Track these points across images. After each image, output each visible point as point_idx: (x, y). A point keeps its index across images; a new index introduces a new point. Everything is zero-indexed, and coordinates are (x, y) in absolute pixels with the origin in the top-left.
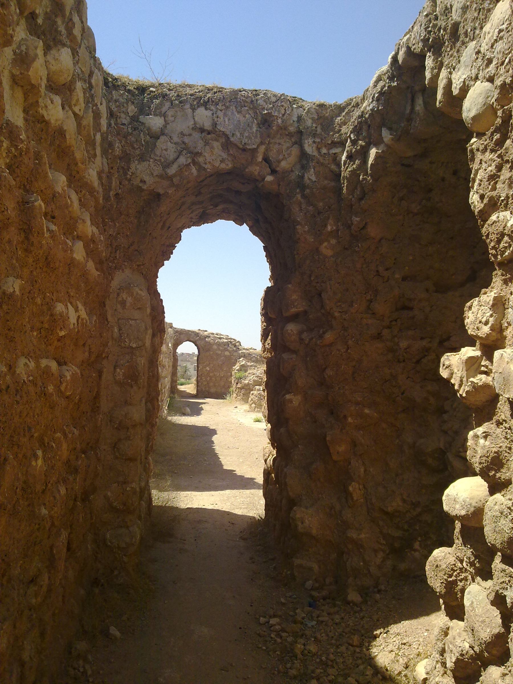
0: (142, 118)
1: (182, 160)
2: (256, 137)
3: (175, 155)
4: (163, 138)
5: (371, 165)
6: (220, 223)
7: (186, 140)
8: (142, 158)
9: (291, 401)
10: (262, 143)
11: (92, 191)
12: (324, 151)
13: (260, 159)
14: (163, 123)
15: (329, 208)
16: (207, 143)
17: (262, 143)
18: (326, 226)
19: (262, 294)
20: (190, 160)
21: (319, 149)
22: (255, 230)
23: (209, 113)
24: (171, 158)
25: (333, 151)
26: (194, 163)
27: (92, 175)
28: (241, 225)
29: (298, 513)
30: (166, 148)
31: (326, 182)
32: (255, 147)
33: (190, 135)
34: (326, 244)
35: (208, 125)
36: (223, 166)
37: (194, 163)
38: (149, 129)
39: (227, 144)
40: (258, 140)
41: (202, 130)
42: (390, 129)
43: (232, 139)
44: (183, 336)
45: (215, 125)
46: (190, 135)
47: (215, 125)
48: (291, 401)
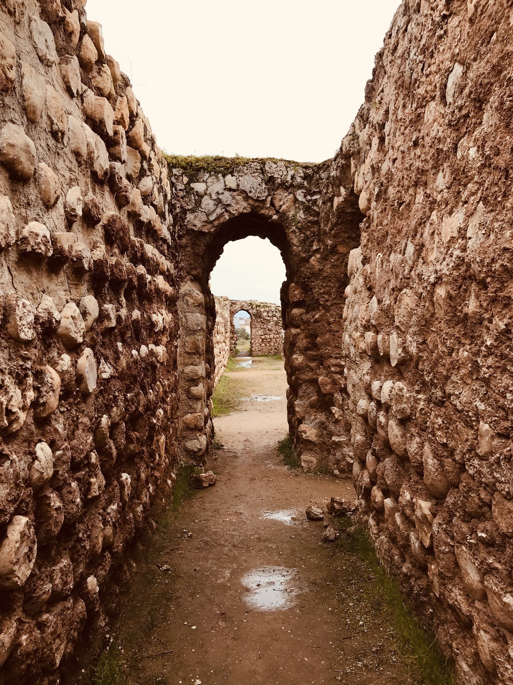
0: (192, 185)
1: (219, 211)
2: (265, 192)
3: (214, 207)
4: (206, 197)
5: (337, 207)
6: (250, 238)
7: (221, 197)
8: (193, 211)
9: (297, 359)
10: (269, 195)
11: (165, 241)
12: (309, 198)
13: (268, 205)
14: (206, 187)
15: (314, 234)
16: (234, 198)
17: (269, 195)
18: (312, 246)
19: (281, 286)
20: (223, 210)
21: (305, 196)
22: (274, 242)
23: (234, 178)
24: (212, 209)
25: (314, 198)
26: (227, 211)
27: (165, 233)
28: (264, 238)
29: (303, 427)
30: (207, 203)
31: (311, 218)
32: (264, 198)
33: (223, 193)
34: (313, 258)
35: (234, 186)
36: (245, 211)
37: (227, 211)
38: (197, 192)
39: (247, 198)
40: (266, 194)
41: (230, 190)
42: (345, 188)
43: (249, 195)
44: (234, 308)
45: (238, 185)
46: (223, 193)
47: (238, 185)
48: (297, 359)
